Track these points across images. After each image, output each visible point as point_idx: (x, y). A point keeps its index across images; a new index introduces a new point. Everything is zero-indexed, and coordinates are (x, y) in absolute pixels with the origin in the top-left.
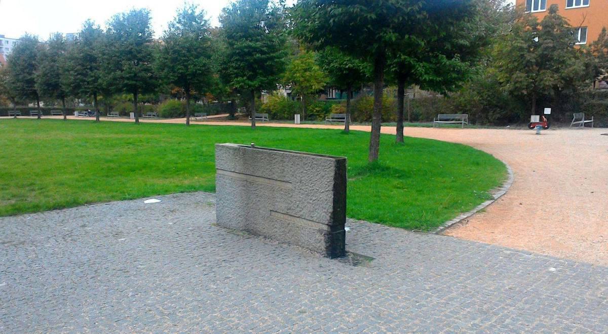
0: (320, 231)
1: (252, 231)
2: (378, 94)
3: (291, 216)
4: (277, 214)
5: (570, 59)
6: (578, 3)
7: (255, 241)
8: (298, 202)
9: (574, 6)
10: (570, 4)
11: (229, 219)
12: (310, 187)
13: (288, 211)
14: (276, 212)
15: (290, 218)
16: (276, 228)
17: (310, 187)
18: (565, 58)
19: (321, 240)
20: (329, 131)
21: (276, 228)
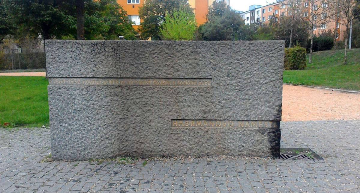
0: (261, 131)
1: (134, 155)
2: (7, 36)
3: (239, 120)
4: (182, 123)
5: (126, 29)
6: (134, 1)
7: (153, 169)
8: (224, 102)
9: (132, 3)
10: (129, 1)
11: (82, 146)
12: (245, 80)
13: (205, 116)
14: (183, 120)
15: (206, 124)
16: (183, 140)
17: (245, 80)
18: (123, 29)
19: (264, 140)
20: (82, 39)
21: (183, 140)
